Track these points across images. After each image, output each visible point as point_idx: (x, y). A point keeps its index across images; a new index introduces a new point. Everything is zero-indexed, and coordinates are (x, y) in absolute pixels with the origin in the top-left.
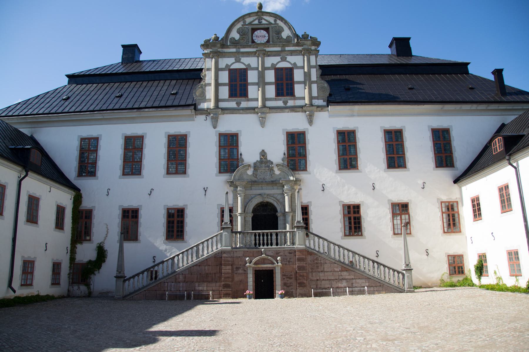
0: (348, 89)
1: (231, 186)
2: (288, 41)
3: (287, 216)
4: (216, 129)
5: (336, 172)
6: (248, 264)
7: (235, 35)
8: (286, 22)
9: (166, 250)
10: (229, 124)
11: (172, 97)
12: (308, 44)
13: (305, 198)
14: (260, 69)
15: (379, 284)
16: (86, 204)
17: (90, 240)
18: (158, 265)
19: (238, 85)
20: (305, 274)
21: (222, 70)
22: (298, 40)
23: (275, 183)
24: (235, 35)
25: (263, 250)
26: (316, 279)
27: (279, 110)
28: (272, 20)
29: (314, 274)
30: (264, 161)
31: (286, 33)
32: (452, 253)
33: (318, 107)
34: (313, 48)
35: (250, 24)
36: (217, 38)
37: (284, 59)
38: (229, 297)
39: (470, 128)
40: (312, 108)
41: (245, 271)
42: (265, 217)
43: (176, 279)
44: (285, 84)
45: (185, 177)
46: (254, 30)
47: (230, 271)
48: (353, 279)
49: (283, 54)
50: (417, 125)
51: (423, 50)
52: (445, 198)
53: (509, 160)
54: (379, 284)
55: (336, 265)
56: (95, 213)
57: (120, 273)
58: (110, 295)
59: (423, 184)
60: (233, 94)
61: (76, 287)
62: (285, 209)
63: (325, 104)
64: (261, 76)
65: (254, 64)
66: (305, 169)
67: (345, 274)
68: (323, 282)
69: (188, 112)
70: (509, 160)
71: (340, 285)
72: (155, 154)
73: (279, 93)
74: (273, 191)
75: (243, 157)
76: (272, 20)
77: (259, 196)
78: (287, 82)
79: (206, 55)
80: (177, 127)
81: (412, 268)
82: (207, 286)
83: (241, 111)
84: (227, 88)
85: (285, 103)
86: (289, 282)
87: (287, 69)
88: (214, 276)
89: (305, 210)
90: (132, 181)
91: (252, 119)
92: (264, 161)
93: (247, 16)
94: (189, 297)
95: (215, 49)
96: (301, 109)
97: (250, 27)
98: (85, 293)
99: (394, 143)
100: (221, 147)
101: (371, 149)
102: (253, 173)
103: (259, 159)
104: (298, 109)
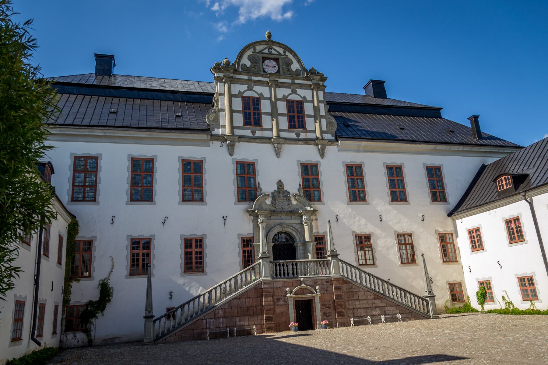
0: (348, 126)
1: (250, 215)
2: (297, 75)
3: (308, 246)
5: (348, 204)
6: (288, 295)
7: (246, 61)
8: (295, 55)
9: (184, 284)
10: (246, 152)
11: (112, 116)
12: (315, 78)
13: (321, 227)
14: (273, 100)
15: (408, 311)
16: (83, 235)
17: (90, 276)
19: (251, 113)
20: (343, 303)
21: (235, 96)
22: (307, 74)
23: (293, 213)
24: (246, 61)
25: (302, 279)
26: (352, 307)
27: (293, 142)
28: (281, 51)
29: (350, 302)
30: (281, 191)
31: (295, 66)
32: (451, 281)
33: (329, 141)
34: (321, 83)
35: (260, 52)
36: (228, 63)
37: (294, 92)
38: (272, 330)
39: (459, 167)
40: (324, 142)
41: (286, 302)
42: (285, 250)
43: (215, 315)
44: (296, 115)
45: (202, 205)
46: (264, 59)
47: (272, 303)
48: (385, 306)
49: (293, 87)
50: (414, 162)
51: (396, 95)
52: (441, 230)
53: (524, 196)
54: (408, 311)
55: (369, 293)
56: (96, 244)
57: (149, 312)
58: (116, 341)
59: (420, 218)
60: (247, 122)
61: (70, 336)
62: (304, 239)
63: (333, 138)
64: (274, 106)
65: (266, 94)
66: (320, 200)
67: (377, 301)
68: (359, 310)
69: (204, 137)
70: (524, 196)
71: (374, 313)
72: (167, 179)
73: (292, 125)
74: (292, 220)
75: (261, 186)
76: (281, 51)
77: (279, 226)
78: (254, 111)
79: (218, 80)
80: (192, 152)
81: (434, 295)
82: (248, 321)
83: (257, 140)
84: (241, 115)
85: (298, 135)
86: (328, 311)
87: (297, 101)
88: (255, 308)
90: (142, 208)
91: (267, 149)
92: (281, 191)
93: (257, 44)
94: (231, 334)
95: (228, 74)
96: (313, 142)
97: (261, 56)
98: (83, 342)
99: (396, 178)
101: (376, 182)
102: (272, 203)
103: (276, 189)
104: (311, 142)
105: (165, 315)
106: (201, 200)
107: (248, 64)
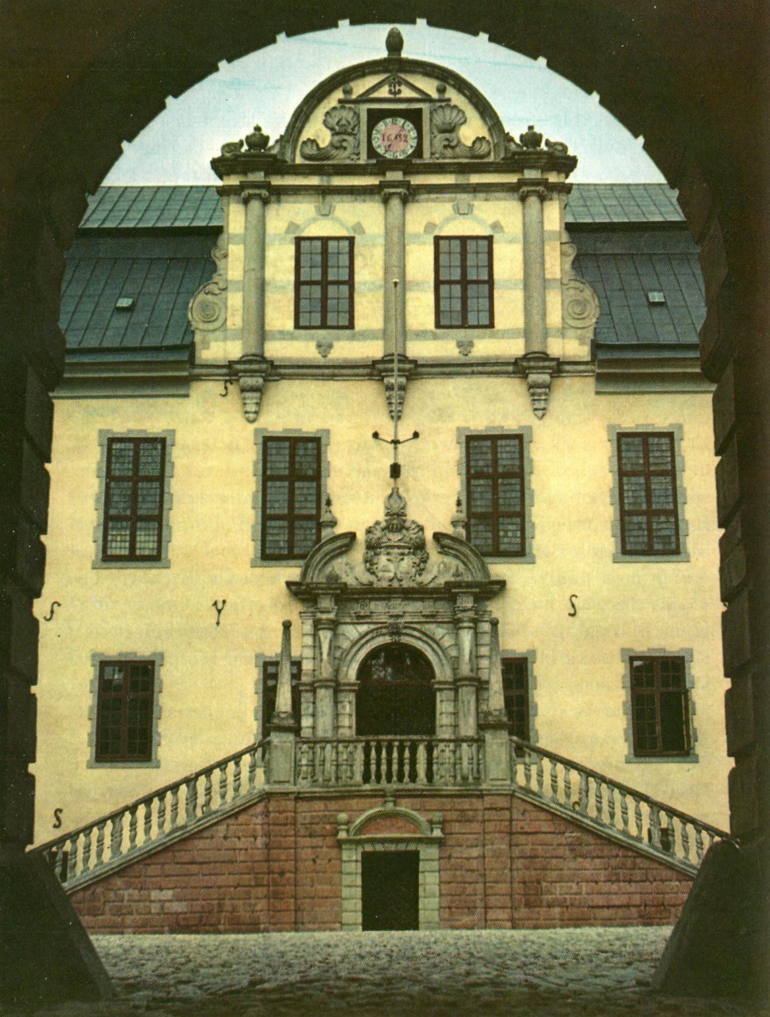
4: (255, 425)
7: (317, 131)
10: (294, 409)
11: (120, 321)
18: (73, 836)
31: (472, 130)
35: (364, 98)
36: (258, 140)
46: (375, 117)
89: (517, 672)
100: (267, 478)
105: (251, 750)
106: (104, 664)
107: (325, 138)
